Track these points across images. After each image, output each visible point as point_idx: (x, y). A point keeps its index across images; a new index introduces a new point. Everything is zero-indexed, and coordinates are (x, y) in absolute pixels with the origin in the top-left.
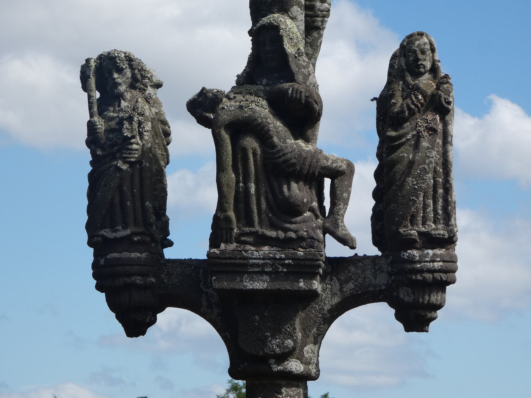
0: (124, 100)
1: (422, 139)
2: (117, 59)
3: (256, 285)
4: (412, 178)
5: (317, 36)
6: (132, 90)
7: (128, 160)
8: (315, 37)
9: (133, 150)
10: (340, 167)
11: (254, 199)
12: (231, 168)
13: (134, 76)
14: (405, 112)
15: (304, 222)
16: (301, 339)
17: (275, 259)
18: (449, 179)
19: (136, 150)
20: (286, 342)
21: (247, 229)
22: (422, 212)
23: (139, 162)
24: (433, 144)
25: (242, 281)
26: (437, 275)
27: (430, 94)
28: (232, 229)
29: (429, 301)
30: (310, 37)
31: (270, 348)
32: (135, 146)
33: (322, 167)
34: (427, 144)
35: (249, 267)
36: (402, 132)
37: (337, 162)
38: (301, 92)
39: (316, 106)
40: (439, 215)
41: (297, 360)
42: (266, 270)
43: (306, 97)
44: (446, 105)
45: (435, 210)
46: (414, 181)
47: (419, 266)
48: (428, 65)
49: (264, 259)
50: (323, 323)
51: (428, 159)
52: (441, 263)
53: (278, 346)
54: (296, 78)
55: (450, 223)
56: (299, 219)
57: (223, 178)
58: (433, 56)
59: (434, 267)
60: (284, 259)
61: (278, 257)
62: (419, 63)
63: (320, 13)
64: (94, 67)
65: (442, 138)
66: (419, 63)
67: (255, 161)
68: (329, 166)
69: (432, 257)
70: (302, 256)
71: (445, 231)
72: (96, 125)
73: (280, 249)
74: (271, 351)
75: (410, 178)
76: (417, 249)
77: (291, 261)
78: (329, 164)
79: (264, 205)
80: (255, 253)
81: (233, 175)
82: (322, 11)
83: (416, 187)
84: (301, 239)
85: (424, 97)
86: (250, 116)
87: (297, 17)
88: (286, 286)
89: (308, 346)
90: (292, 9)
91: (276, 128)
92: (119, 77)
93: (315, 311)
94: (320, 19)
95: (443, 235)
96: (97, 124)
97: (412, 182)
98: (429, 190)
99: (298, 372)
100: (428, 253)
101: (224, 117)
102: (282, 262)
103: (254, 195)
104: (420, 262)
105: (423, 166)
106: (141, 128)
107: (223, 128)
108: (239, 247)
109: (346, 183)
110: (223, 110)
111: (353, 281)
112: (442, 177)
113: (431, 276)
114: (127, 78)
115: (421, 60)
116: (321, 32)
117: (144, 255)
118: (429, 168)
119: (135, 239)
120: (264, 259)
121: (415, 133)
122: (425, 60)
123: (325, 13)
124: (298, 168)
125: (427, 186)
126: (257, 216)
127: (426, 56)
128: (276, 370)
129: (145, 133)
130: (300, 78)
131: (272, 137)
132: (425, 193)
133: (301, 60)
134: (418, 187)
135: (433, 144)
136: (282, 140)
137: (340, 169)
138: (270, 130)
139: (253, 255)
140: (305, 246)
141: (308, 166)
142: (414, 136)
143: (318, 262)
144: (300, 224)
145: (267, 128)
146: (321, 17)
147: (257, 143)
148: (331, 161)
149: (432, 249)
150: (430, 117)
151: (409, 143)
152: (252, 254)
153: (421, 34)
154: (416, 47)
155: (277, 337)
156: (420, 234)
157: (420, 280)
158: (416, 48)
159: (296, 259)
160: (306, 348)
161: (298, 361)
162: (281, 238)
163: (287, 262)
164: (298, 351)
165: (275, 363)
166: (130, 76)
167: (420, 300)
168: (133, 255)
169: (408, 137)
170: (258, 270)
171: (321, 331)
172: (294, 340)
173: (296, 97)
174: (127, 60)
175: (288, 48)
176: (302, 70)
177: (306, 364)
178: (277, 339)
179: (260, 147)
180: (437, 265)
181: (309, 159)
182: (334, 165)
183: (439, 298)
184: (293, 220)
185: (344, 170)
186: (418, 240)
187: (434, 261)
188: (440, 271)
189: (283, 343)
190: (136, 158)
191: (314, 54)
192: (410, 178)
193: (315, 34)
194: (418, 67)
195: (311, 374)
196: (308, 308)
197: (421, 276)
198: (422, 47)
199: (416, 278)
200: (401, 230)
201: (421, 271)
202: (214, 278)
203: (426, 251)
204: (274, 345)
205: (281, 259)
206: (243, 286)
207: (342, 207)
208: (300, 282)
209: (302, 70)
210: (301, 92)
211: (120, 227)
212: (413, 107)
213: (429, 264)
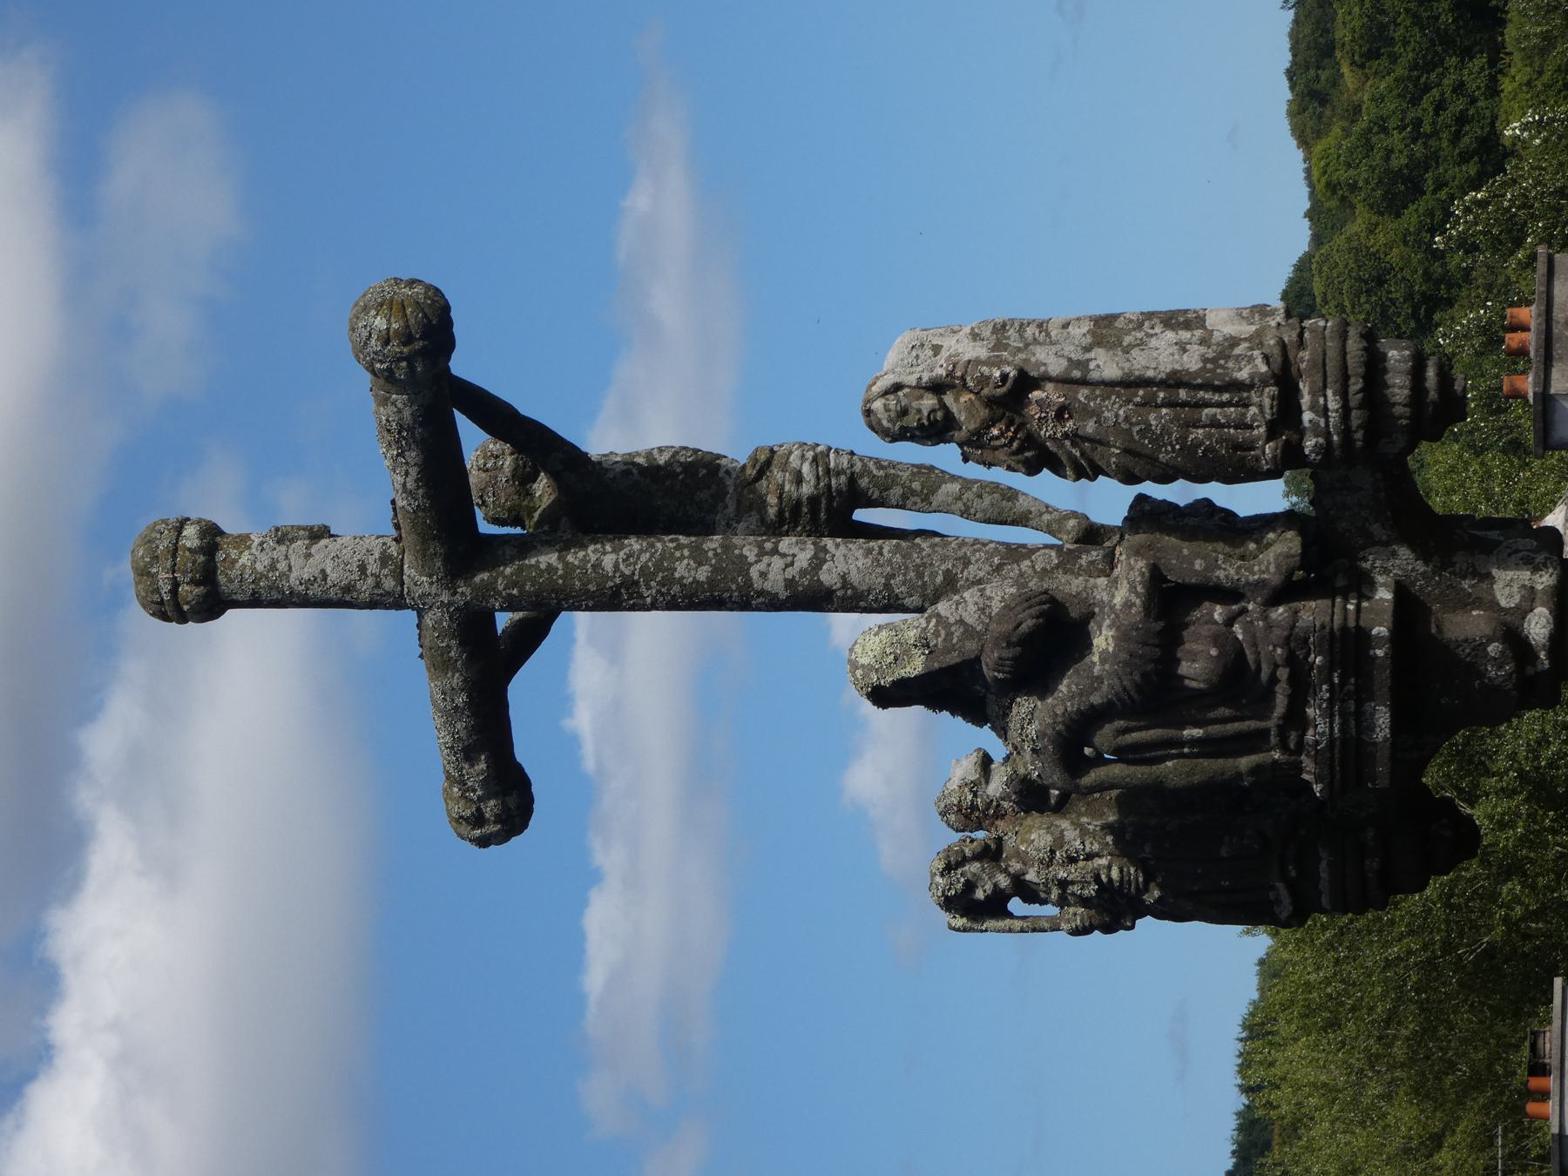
0: (1024, 874)
1: (1080, 432)
2: (949, 894)
3: (1383, 722)
4: (1160, 452)
5: (866, 480)
6: (1004, 856)
7: (1141, 886)
8: (869, 483)
9: (1122, 878)
10: (1142, 574)
11: (1215, 729)
12: (1154, 767)
13: (977, 857)
14: (1026, 457)
15: (1255, 645)
16: (1485, 611)
17: (1331, 701)
18: (1157, 380)
19: (1121, 871)
20: (1493, 654)
21: (1273, 740)
22: (1226, 430)
23: (1141, 864)
24: (1087, 413)
25: (1375, 744)
26: (1355, 400)
27: (987, 411)
28: (1275, 762)
29: (1405, 405)
30: (870, 492)
31: (1503, 681)
32: (1115, 874)
33: (1145, 615)
34: (1090, 424)
35: (1348, 735)
36: (1064, 459)
37: (1134, 581)
38: (1000, 659)
39: (1024, 627)
40: (1232, 399)
41: (1527, 620)
42: (1352, 709)
43: (1009, 645)
44: (1009, 384)
45: (1221, 405)
46: (1166, 450)
47: (1335, 438)
48: (929, 402)
49: (1332, 716)
50: (1451, 567)
51: (1120, 424)
52: (1329, 393)
53: (1501, 667)
54: (973, 657)
55: (1248, 382)
56: (1250, 657)
57: (1174, 782)
58: (909, 387)
59: (1337, 411)
60: (1332, 684)
61: (1328, 695)
62: (926, 423)
63: (822, 484)
64: (965, 920)
65: (1076, 386)
66: (926, 423)
67: (1139, 729)
68: (1143, 602)
69: (1316, 413)
70: (1324, 658)
71: (1263, 390)
72: (1077, 927)
73: (1311, 691)
74: (1510, 678)
75: (1161, 456)
76: (1301, 440)
77: (1336, 675)
78: (1138, 602)
79: (1224, 711)
80: (1320, 729)
81: (1169, 764)
82: (818, 478)
83: (1178, 447)
84: (1291, 660)
85: (993, 422)
86: (1053, 742)
87: (842, 574)
88: (1383, 678)
89: (1499, 597)
90: (827, 584)
91: (1073, 697)
92: (983, 886)
93: (1428, 586)
94: (833, 482)
95: (1273, 399)
96: (1074, 926)
97: (1167, 452)
98: (1182, 419)
99: (1551, 620)
100: (1310, 421)
101: (1055, 778)
102: (1337, 688)
103: (1205, 728)
104: (1328, 435)
105: (1135, 434)
106: (1078, 856)
107: (1078, 780)
108: (1309, 752)
109: (1174, 562)
110: (1042, 776)
111: (1367, 524)
112: (1155, 389)
113: (1354, 413)
114: (983, 869)
115: (919, 420)
116: (858, 471)
117: (1324, 854)
118: (1138, 423)
119: (1293, 874)
120: (1332, 716)
121: (1068, 443)
122: (919, 411)
123: (820, 469)
124: (1150, 667)
125: (1175, 422)
126: (1247, 723)
127: (912, 407)
128: (1546, 662)
129: (1087, 850)
130: (971, 646)
131: (1092, 706)
132: (1188, 426)
133: (935, 641)
134: (1177, 443)
135: (1087, 413)
136: (1096, 685)
137: (1147, 574)
138: (1078, 708)
139: (1324, 732)
140: (1304, 651)
141: (1147, 648)
142: (1074, 444)
143: (1335, 631)
144: (1260, 654)
145: (1074, 716)
146: (830, 479)
147: (1104, 726)
148: (1133, 595)
149: (1301, 412)
150: (1033, 411)
151: (1088, 451)
152: (1322, 734)
153: (868, 413)
154: (894, 425)
155: (1482, 668)
156: (1272, 435)
157: (1364, 435)
158: (897, 428)
159: (1330, 667)
160: (1503, 603)
161: (1528, 617)
162: (1290, 692)
163: (1336, 680)
164: (1508, 618)
165: (1534, 666)
166: (977, 865)
167: (1404, 423)
168: (1324, 875)
169: (1078, 454)
170: (1353, 722)
171: (1468, 569)
172: (1487, 640)
173: (1011, 667)
174: (949, 873)
175: (915, 669)
176: (955, 641)
177: (1534, 598)
178: (1487, 670)
179: (1111, 721)
180: (1333, 403)
181: (1131, 646)
182: (1139, 589)
183: (1398, 381)
184: (1253, 667)
185: (1147, 565)
186: (1284, 437)
187: (1326, 409)
188: (1344, 394)
189: (1495, 659)
190: (1136, 871)
191: (902, 482)
192: (1161, 456)
193: (864, 482)
194: (933, 423)
195: (1552, 587)
196: (1422, 598)
197: (1356, 432)
198: (893, 414)
199: (1359, 440)
200: (1265, 468)
201: (1346, 433)
202: (1369, 785)
203: (1306, 424)
204: (1499, 673)
205: (1331, 690)
206: (1385, 742)
207: (1222, 572)
208: (1375, 654)
209: (955, 641)
210: (1000, 659)
211: (1270, 894)
212: (1015, 445)
213: (1332, 420)
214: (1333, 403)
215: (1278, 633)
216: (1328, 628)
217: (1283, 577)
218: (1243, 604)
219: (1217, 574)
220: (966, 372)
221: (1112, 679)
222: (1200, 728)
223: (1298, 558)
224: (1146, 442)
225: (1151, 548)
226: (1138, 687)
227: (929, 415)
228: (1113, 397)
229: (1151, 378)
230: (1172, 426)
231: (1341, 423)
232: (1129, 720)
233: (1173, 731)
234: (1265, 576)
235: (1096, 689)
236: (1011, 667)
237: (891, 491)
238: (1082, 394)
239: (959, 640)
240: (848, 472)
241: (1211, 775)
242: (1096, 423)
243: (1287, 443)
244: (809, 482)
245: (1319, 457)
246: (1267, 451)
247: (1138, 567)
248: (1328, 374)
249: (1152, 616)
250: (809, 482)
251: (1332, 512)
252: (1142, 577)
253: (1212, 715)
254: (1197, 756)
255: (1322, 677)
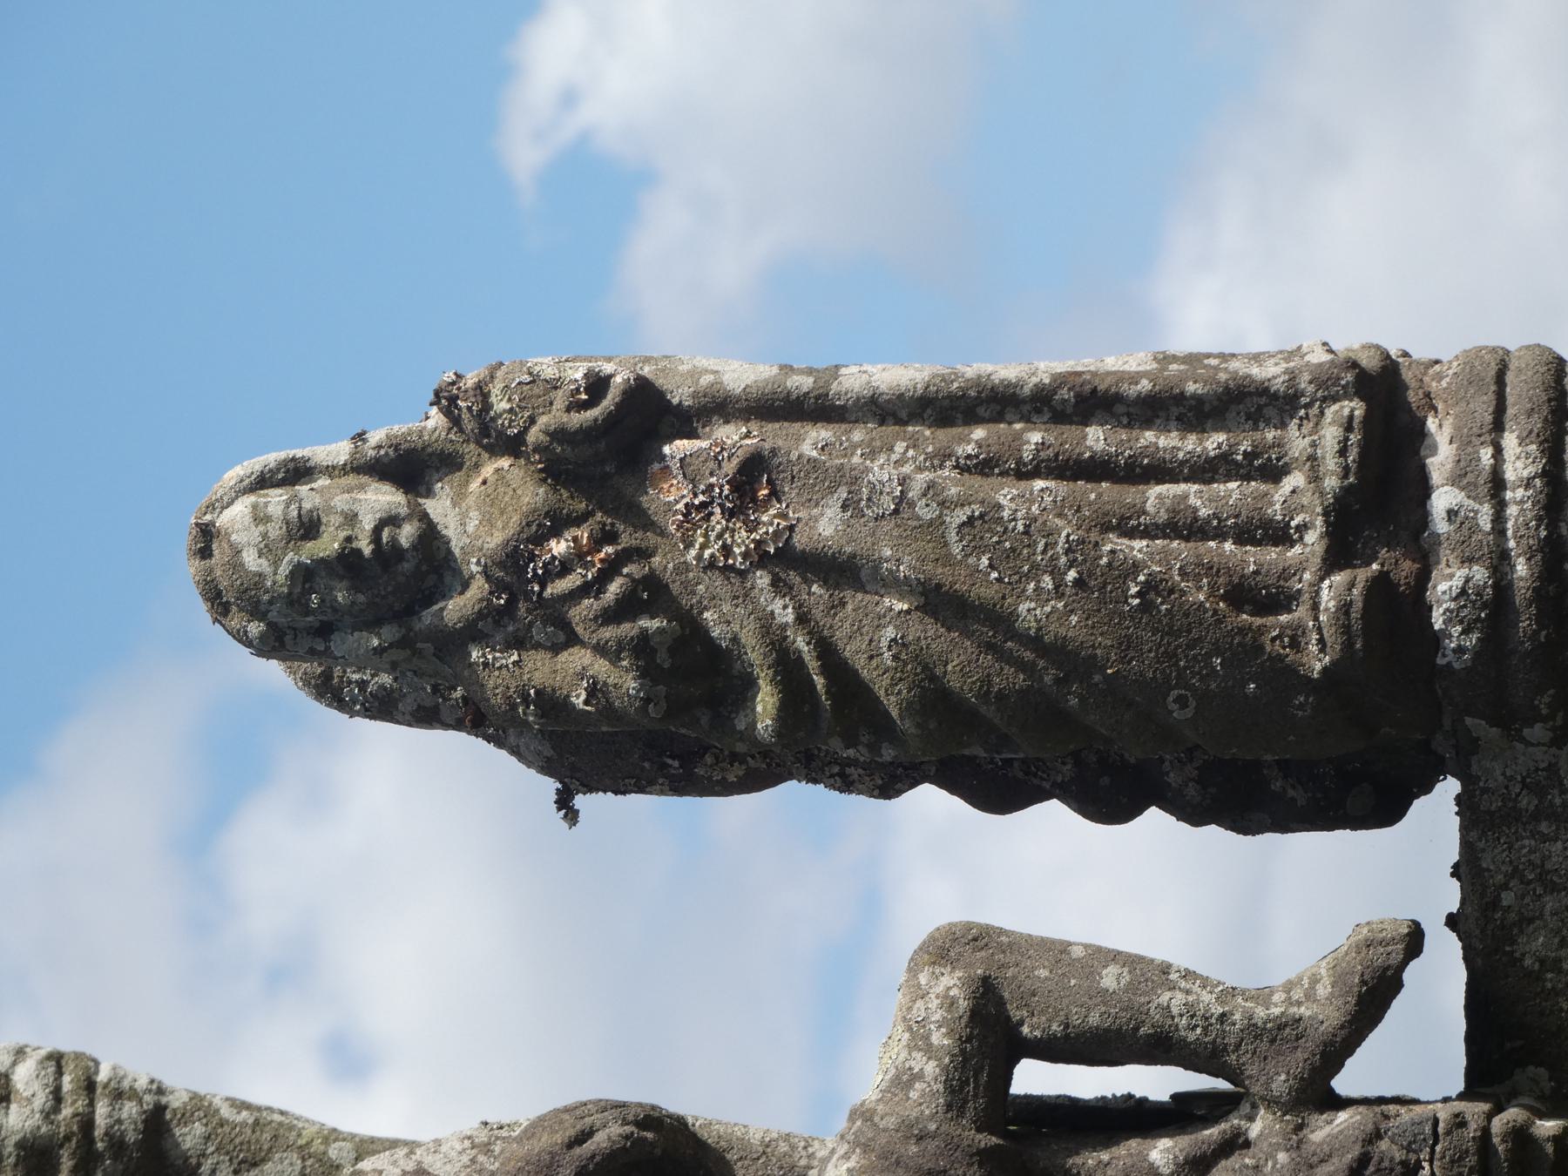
1: (800, 541)
8: (208, 1138)
10: (951, 1003)
14: (644, 634)
18: (1027, 390)
22: (1212, 544)
27: (541, 491)
33: (949, 1107)
34: (829, 513)
36: (755, 654)
44: (609, 402)
45: (1206, 470)
47: (1521, 568)
48: (381, 498)
51: (912, 505)
52: (1510, 441)
59: (1528, 484)
68: (945, 1069)
69: (1469, 489)
71: (1322, 413)
75: (1023, 608)
76: (1423, 578)
78: (931, 1068)
82: (57, 1096)
83: (1072, 575)
94: (102, 1110)
100: (1451, 514)
104: (1500, 561)
105: (952, 536)
109: (1043, 973)
112: (1018, 426)
121: (762, 579)
122: (351, 518)
123: (66, 1079)
127: (330, 510)
134: (1072, 564)
146: (92, 1104)
148: (918, 1055)
151: (817, 613)
154: (276, 564)
158: (284, 569)
182: (939, 1038)
185: (965, 982)
186: (1375, 566)
187: (1497, 484)
191: (301, 1142)
192: (1023, 608)
198: (275, 531)
200: (1318, 666)
212: (614, 588)
213: (1512, 511)
214: (1519, 464)
216: (1473, 1126)
218: (1236, 1122)
219: (1164, 998)
220: (492, 377)
224: (985, 561)
227: (377, 531)
228: (900, 447)
229: (1009, 385)
230: (1059, 522)
231: (1539, 519)
234: (1303, 1011)
238: (811, 440)
242: (844, 507)
243: (1380, 586)
245: (1474, 637)
246: (1325, 594)
247: (940, 989)
248: (1510, 400)
249: (970, 1113)
250: (29, 1100)
251: (1507, 898)
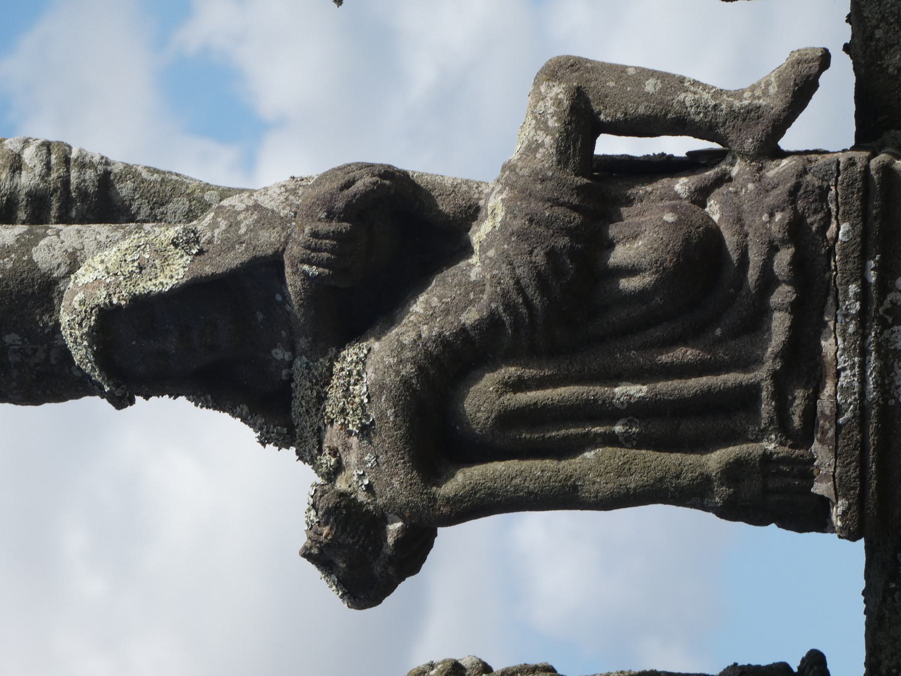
10: (559, 103)
11: (667, 387)
12: (564, 463)
15: (739, 221)
17: (863, 317)
21: (766, 408)
28: (766, 457)
33: (559, 162)
37: (543, 114)
38: (315, 234)
49: (864, 353)
54: (270, 252)
56: (730, 239)
57: (596, 486)
60: (865, 285)
67: (541, 383)
68: (557, 141)
73: (831, 300)
79: (686, 354)
80: (843, 381)
82: (48, 166)
86: (395, 401)
87: (70, 250)
90: (44, 267)
94: (74, 174)
103: (652, 386)
107: (434, 488)
109: (612, 84)
110: (377, 489)
116: (116, 171)
123: (53, 157)
124: (563, 241)
126: (724, 377)
130: (268, 240)
133: (209, 234)
136: (472, 296)
139: (850, 386)
140: (820, 216)
141: (558, 211)
144: (747, 235)
146: (68, 171)
148: (540, 133)
152: (846, 390)
163: (872, 277)
173: (331, 251)
175: (172, 277)
176: (243, 230)
179: (494, 368)
181: (533, 205)
182: (552, 123)
184: (734, 257)
185: (567, 91)
191: (188, 191)
193: (125, 189)
205: (863, 296)
209: (243, 230)
210: (315, 234)
215: (778, 194)
216: (859, 165)
217: (790, 95)
219: (682, 96)
221: (500, 268)
222: (643, 385)
223: (817, 63)
225: (575, 68)
226: (541, 279)
232: (526, 366)
233: (598, 388)
235: (471, 302)
236: (331, 251)
237: (170, 205)
239: (249, 230)
240: (100, 167)
241: (659, 475)
244: (32, 169)
247: (553, 94)
252: (558, 107)
253: (664, 358)
254: (642, 442)
255: (850, 266)
